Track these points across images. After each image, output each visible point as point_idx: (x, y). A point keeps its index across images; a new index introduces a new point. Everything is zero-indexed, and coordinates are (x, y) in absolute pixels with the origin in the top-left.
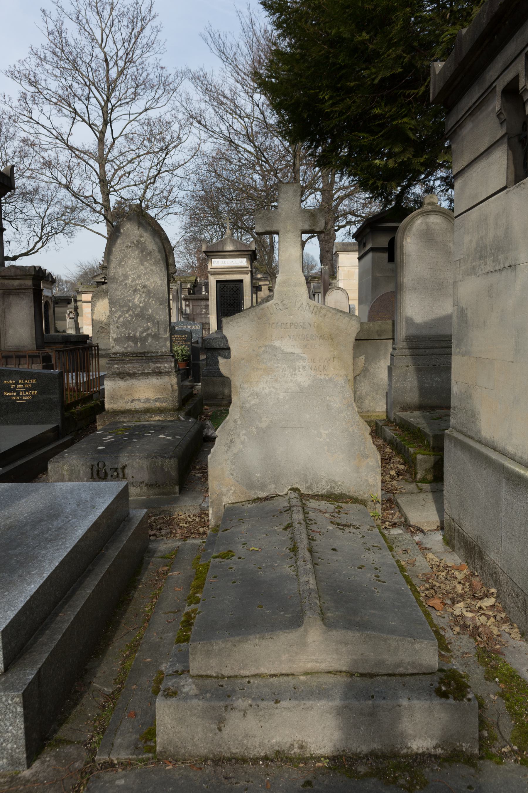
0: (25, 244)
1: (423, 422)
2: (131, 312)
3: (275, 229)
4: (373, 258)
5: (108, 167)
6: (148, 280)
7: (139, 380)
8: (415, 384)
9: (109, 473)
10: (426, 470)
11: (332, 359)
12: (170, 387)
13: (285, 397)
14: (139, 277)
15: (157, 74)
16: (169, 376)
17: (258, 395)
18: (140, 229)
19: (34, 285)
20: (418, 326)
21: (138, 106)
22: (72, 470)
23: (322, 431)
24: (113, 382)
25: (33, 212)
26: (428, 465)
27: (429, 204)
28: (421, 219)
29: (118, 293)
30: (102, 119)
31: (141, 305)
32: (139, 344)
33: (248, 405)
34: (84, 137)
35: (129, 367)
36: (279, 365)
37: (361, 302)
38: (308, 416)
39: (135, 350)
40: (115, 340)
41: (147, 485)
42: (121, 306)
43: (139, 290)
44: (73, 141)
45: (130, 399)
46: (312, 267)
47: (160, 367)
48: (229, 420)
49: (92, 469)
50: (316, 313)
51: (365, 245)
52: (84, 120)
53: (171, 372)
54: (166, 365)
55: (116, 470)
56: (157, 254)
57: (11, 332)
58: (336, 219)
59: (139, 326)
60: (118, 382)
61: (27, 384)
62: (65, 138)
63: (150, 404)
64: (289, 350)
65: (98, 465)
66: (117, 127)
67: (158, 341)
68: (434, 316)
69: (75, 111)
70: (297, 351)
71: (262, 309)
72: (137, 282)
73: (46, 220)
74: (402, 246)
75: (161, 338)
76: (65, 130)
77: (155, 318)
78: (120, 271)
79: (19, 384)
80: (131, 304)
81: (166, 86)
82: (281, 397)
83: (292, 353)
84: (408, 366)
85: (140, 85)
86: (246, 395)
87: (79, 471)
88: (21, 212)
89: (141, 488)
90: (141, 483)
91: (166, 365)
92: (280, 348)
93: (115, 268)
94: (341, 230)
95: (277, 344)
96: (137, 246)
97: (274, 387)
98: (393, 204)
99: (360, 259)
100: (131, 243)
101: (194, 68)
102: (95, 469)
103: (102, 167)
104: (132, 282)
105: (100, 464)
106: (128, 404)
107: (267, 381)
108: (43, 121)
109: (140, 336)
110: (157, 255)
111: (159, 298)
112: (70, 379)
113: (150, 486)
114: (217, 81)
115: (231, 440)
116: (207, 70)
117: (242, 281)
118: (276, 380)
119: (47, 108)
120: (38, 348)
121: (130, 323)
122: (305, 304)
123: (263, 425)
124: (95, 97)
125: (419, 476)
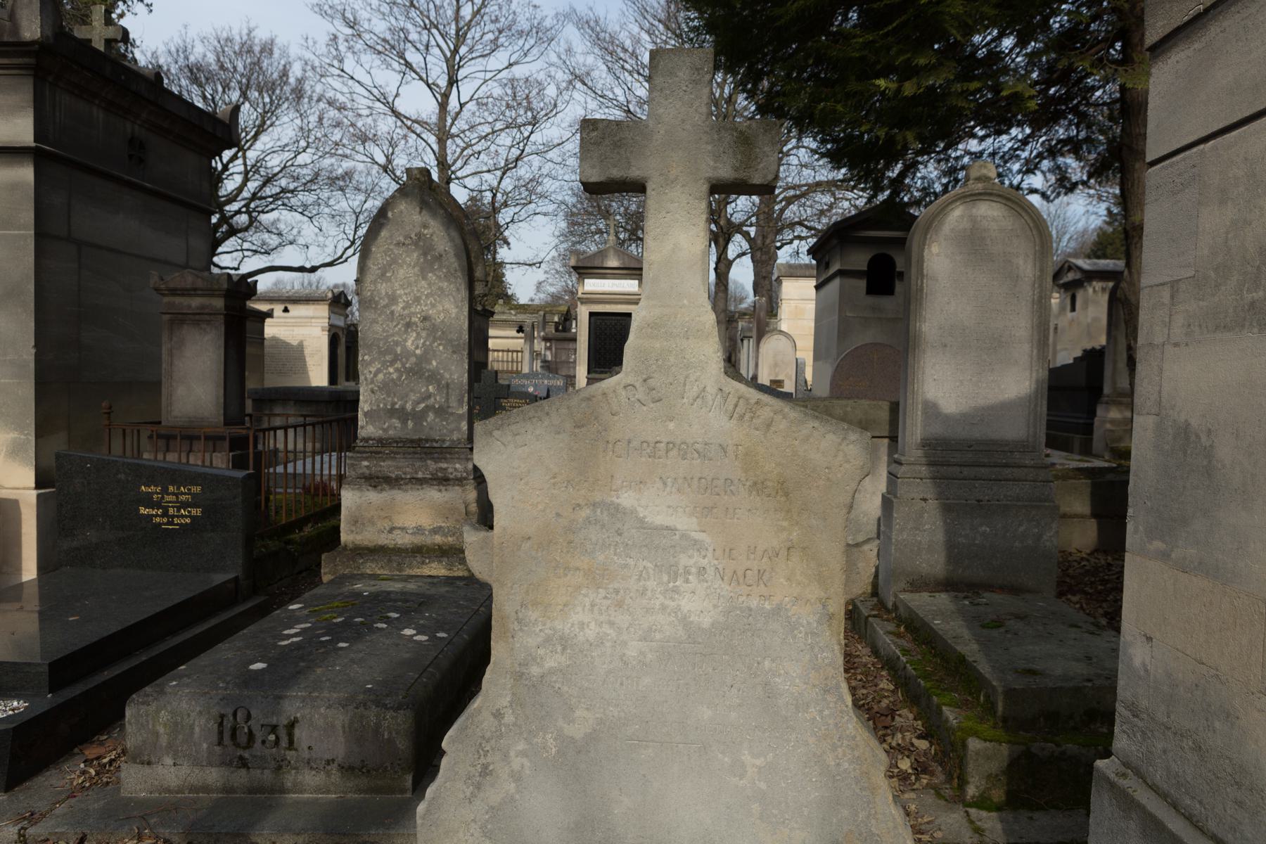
0: (330, 249)
1: (966, 634)
2: (398, 365)
3: (634, 173)
4: (841, 286)
5: (450, 145)
6: (433, 306)
7: (406, 491)
8: (940, 537)
9: (259, 735)
10: (989, 776)
11: (783, 553)
12: (462, 508)
13: (642, 653)
14: (417, 300)
15: (527, 15)
16: (462, 486)
17: (565, 642)
18: (424, 212)
19: (226, 307)
20: (947, 419)
21: (499, 60)
22: (176, 724)
23: (746, 758)
24: (358, 494)
25: (344, 204)
26: (994, 767)
27: (978, 179)
28: (961, 208)
29: (378, 328)
30: (446, 77)
31: (418, 352)
32: (410, 424)
33: (535, 670)
34: (418, 102)
35: (387, 467)
36: (631, 562)
37: (817, 357)
38: (707, 713)
39: (402, 435)
40: (366, 414)
41: (341, 767)
42: (380, 353)
43: (415, 323)
44: (400, 106)
45: (387, 525)
46: (742, 300)
47: (446, 469)
48: (479, 710)
49: (221, 724)
50: (742, 417)
51: (827, 266)
52: (421, 78)
53: (465, 479)
54: (458, 466)
55: (274, 728)
56: (453, 260)
57: (180, 391)
58: (779, 231)
59: (412, 391)
60: (367, 493)
61: (182, 493)
62: (390, 100)
63: (423, 538)
64: (659, 520)
65: (235, 715)
66: (466, 90)
67: (446, 420)
68: (981, 402)
69: (408, 65)
70: (684, 522)
71: (589, 399)
72: (413, 310)
73: (361, 217)
74: (921, 261)
75: (452, 414)
76: (391, 90)
77: (442, 376)
78: (383, 288)
79: (168, 494)
80: (399, 350)
81: (541, 34)
82: (632, 652)
83: (668, 528)
84: (925, 500)
85: (507, 30)
86: (531, 642)
87: (192, 727)
88: (328, 206)
89: (328, 774)
90: (328, 762)
91: (458, 466)
92: (633, 511)
93: (374, 282)
94: (786, 247)
95: (626, 499)
96: (416, 244)
97: (611, 624)
98: (887, 193)
99: (818, 288)
100: (407, 237)
101: (582, 10)
102: (228, 724)
103: (442, 142)
104: (404, 308)
105: (239, 714)
106: (383, 536)
107: (593, 605)
108: (360, 75)
109: (413, 409)
110: (453, 262)
111: (451, 341)
112: (326, 466)
113: (348, 769)
114: (613, 27)
115: (485, 767)
116: (600, 12)
117: (629, 315)
118: (620, 605)
119: (368, 58)
120: (227, 422)
121: (396, 385)
122: (712, 390)
123: (577, 731)
124: (438, 45)
125: (971, 791)
